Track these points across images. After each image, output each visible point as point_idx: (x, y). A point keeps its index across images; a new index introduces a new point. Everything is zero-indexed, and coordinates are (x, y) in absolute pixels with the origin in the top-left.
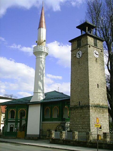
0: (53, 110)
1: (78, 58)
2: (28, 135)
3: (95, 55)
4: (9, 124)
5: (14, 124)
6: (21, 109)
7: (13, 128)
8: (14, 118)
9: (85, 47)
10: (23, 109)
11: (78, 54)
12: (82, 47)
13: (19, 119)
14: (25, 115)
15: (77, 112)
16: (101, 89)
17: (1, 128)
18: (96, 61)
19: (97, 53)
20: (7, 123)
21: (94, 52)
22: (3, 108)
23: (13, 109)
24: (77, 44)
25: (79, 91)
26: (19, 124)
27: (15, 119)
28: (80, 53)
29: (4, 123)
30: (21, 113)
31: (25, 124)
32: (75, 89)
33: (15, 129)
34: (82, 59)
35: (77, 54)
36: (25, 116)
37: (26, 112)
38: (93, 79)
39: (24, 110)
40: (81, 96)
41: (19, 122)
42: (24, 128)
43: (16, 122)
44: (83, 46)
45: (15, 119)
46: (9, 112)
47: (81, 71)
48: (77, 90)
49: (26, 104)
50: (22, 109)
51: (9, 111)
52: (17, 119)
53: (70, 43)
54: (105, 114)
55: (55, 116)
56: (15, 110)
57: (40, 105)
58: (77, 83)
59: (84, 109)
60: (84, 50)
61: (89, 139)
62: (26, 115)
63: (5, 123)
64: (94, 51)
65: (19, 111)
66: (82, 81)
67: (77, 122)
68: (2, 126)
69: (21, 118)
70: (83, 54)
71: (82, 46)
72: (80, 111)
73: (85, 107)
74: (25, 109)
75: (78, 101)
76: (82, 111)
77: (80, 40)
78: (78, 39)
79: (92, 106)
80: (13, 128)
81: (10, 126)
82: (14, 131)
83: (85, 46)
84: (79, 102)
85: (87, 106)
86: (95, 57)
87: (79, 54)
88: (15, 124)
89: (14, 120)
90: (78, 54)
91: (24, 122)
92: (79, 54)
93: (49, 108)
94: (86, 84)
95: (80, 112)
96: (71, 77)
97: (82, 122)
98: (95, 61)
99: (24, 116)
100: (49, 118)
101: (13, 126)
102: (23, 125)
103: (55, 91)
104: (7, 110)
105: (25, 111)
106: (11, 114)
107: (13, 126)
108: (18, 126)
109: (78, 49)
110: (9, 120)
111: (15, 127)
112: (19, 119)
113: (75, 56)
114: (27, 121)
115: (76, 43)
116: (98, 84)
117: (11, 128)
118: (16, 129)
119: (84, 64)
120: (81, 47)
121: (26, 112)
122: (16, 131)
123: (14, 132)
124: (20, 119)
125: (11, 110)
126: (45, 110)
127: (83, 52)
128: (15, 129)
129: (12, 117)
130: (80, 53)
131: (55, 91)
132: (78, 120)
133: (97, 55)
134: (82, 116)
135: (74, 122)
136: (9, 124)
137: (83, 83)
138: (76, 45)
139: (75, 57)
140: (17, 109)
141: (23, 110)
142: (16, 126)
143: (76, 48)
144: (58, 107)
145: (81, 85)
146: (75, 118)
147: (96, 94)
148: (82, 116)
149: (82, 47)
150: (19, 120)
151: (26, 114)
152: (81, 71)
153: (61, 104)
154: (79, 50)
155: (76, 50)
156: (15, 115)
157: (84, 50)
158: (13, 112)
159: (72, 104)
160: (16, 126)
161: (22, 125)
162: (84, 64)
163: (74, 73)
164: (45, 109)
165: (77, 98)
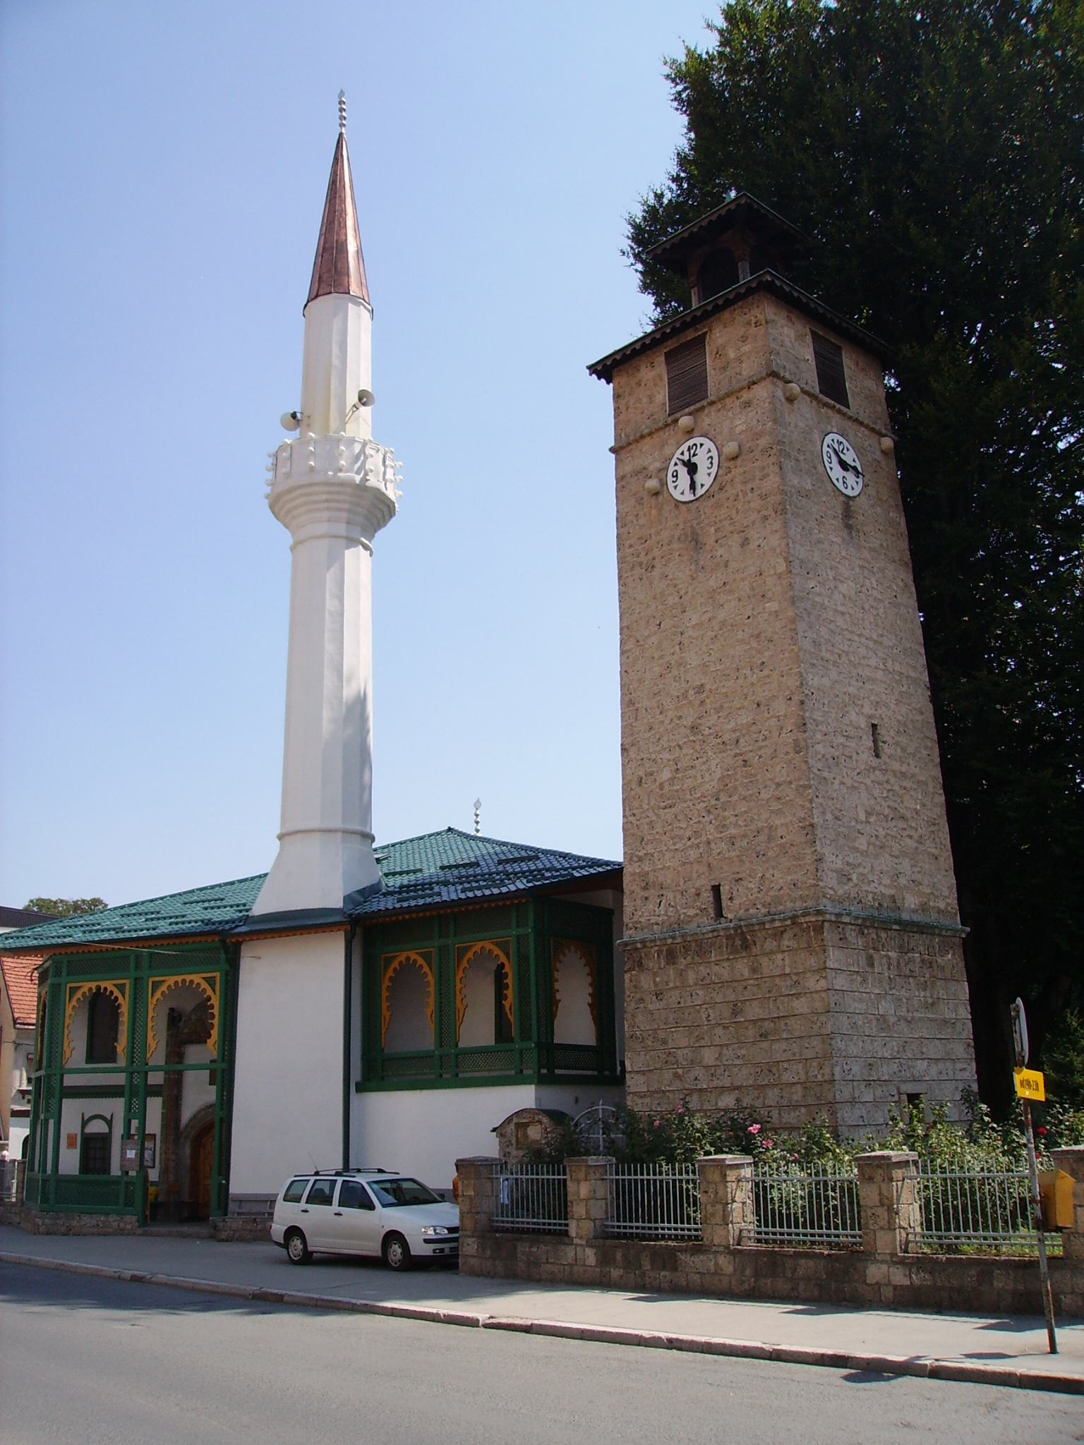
0: (460, 974)
1: (689, 497)
2: (241, 1200)
3: (836, 473)
4: (72, 1111)
5: (115, 1107)
6: (171, 980)
7: (105, 1139)
8: (115, 1061)
9: (748, 404)
10: (192, 977)
11: (683, 472)
12: (721, 399)
13: (156, 1069)
14: (206, 1027)
15: (704, 983)
16: (895, 765)
17: (14, 1152)
18: (849, 527)
19: (849, 457)
20: (54, 1102)
21: (825, 449)
22: (23, 989)
23: (103, 984)
24: (671, 382)
25: (711, 785)
26: (155, 1107)
27: (122, 1061)
28: (705, 454)
29: (28, 1108)
30: (174, 1018)
31: (211, 1106)
32: (666, 775)
33: (122, 1156)
34: (724, 510)
35: (671, 469)
36: (211, 1042)
37: (215, 1001)
38: (834, 674)
39: (204, 985)
40: (733, 831)
41: (154, 1091)
42: (206, 1141)
43: (135, 1093)
44: (728, 395)
45: (122, 1061)
46: (69, 1011)
47: (722, 615)
48: (689, 783)
49: (215, 932)
50: (179, 978)
51: (74, 1002)
52: (137, 1065)
53: (604, 390)
54: (942, 994)
55: (477, 1029)
56: (121, 988)
57: (27, 1120)
58: (688, 722)
59: (770, 944)
60: (740, 424)
61: (891, 1228)
62: (215, 1033)
63: (36, 1107)
64: (828, 440)
65: (158, 995)
66: (737, 703)
67: (698, 1072)
68: (18, 1133)
69: (176, 1053)
70: (734, 458)
71: (713, 389)
72: (724, 972)
73: (779, 934)
74: (211, 981)
75: (705, 883)
76: (742, 968)
77: (700, 342)
78: (671, 344)
79: (838, 915)
80: (105, 1139)
81: (85, 1123)
82: (115, 1170)
83: (745, 396)
84: (716, 889)
85: (794, 918)
86: (840, 485)
87: (692, 468)
88: (129, 1108)
89: (120, 1079)
90: (685, 464)
91: (198, 1094)
92: (692, 468)
93: (421, 961)
94: (773, 722)
95: (726, 977)
96: (624, 673)
97: (745, 1071)
98: (837, 523)
99: (202, 1038)
100: (426, 1041)
101: (110, 1123)
102: (190, 1121)
103: (450, 829)
104: (56, 991)
105: (209, 992)
106: (85, 1023)
107: (110, 1123)
108: (154, 1124)
109: (685, 421)
110: (70, 1080)
111: (127, 1136)
112: (156, 1069)
113: (652, 483)
114: (224, 1075)
115: (654, 378)
116: (874, 726)
117: (94, 1149)
118: (131, 1154)
119: (745, 542)
120: (712, 403)
121: (215, 1001)
122: (152, 1198)
123: (117, 1181)
124: (162, 1063)
125: (88, 986)
126: (386, 983)
127: (731, 448)
128: (123, 1154)
129: (100, 1050)
130: (701, 460)
131: (450, 829)
132: (709, 1056)
133: (850, 477)
134: (754, 1011)
135: (668, 1075)
136: (72, 1111)
137: (745, 718)
138: (662, 395)
139: (657, 494)
140: (141, 987)
141: (189, 988)
142: (135, 1123)
143: (662, 417)
144: (503, 946)
145: (726, 737)
146: (680, 1039)
147: (868, 814)
148: (754, 1011)
149: (721, 399)
150: (161, 1074)
151: (216, 1021)
152: (722, 615)
153: (531, 923)
154: (690, 433)
155: (665, 435)
156: (125, 1019)
157: (740, 424)
158: (101, 1012)
159: (641, 914)
160: (135, 1123)
161: (187, 1114)
162: (745, 542)
163: (654, 639)
164: (390, 973)
165: (693, 854)
